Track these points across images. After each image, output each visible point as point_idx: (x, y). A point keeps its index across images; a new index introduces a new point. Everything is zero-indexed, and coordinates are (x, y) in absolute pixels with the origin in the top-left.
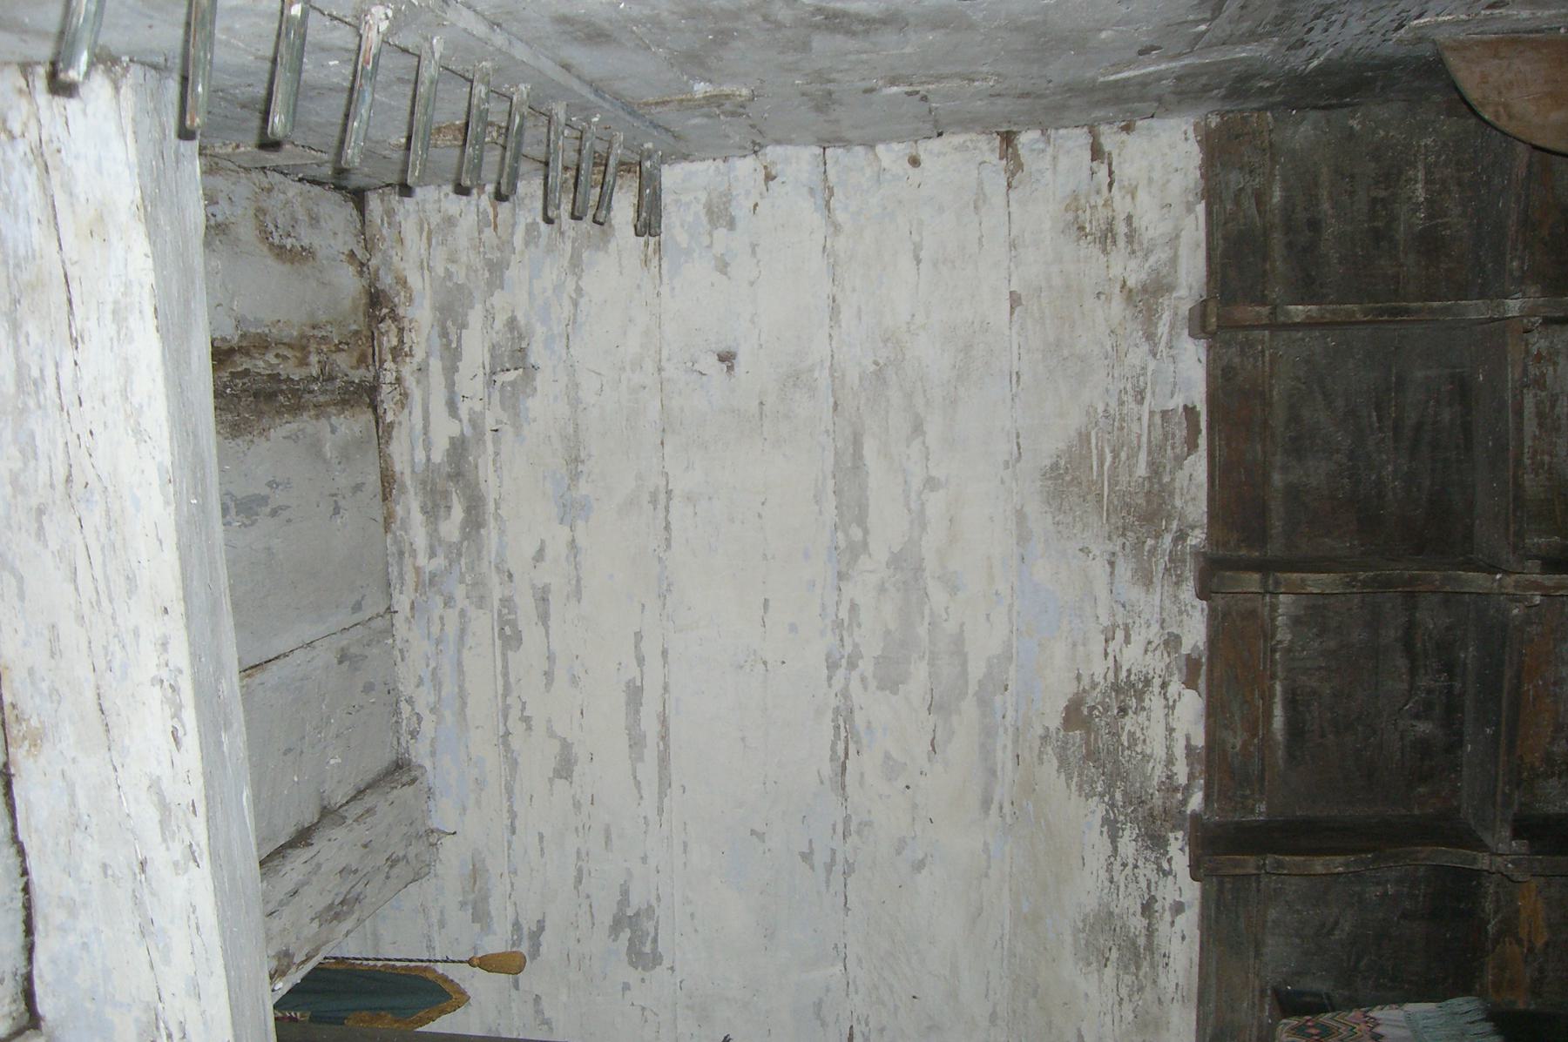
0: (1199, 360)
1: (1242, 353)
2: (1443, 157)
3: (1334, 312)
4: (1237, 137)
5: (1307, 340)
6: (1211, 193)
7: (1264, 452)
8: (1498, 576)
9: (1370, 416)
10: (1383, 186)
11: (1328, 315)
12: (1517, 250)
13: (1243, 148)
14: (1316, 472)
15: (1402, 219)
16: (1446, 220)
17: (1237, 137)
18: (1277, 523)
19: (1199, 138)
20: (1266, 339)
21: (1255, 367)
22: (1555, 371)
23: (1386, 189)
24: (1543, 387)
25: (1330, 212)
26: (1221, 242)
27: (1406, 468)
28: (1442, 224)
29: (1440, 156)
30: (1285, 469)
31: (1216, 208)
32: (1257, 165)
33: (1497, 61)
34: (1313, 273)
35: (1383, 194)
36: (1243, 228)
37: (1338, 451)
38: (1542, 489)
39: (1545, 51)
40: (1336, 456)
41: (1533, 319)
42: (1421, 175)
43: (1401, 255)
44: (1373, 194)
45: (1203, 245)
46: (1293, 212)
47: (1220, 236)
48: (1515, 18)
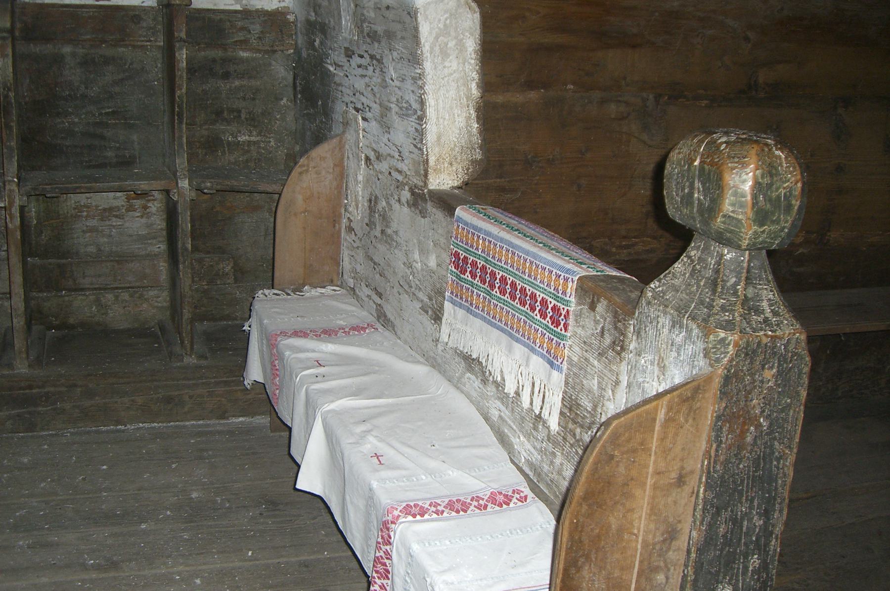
0: (143, 2)
1: (149, 28)
2: (263, 152)
3: (181, 77)
4: (281, 31)
5: (156, 70)
6: (247, 14)
7: (85, 41)
8: (16, 180)
9: (109, 108)
10: (248, 117)
11: (180, 73)
12: (217, 185)
13: (274, 34)
14: (72, 74)
15: (229, 128)
16: (227, 152)
17: (281, 31)
18: (38, 49)
19: (280, 9)
20: (158, 44)
21: (140, 36)
22: (137, 217)
23: (246, 118)
24: (128, 210)
25: (233, 85)
26: (219, 18)
27: (77, 129)
28: (224, 150)
29: (263, 149)
30: (74, 55)
31: (240, 16)
32: (263, 42)
33: (332, 165)
34: (196, 74)
35: (243, 116)
36: (227, 31)
37: (86, 88)
38: (66, 212)
39: (336, 192)
40: (83, 86)
41: (176, 195)
42: (253, 139)
43: (206, 127)
44: (243, 111)
45: (215, 8)
46: (234, 63)
47: (222, 17)
48: (358, 173)
